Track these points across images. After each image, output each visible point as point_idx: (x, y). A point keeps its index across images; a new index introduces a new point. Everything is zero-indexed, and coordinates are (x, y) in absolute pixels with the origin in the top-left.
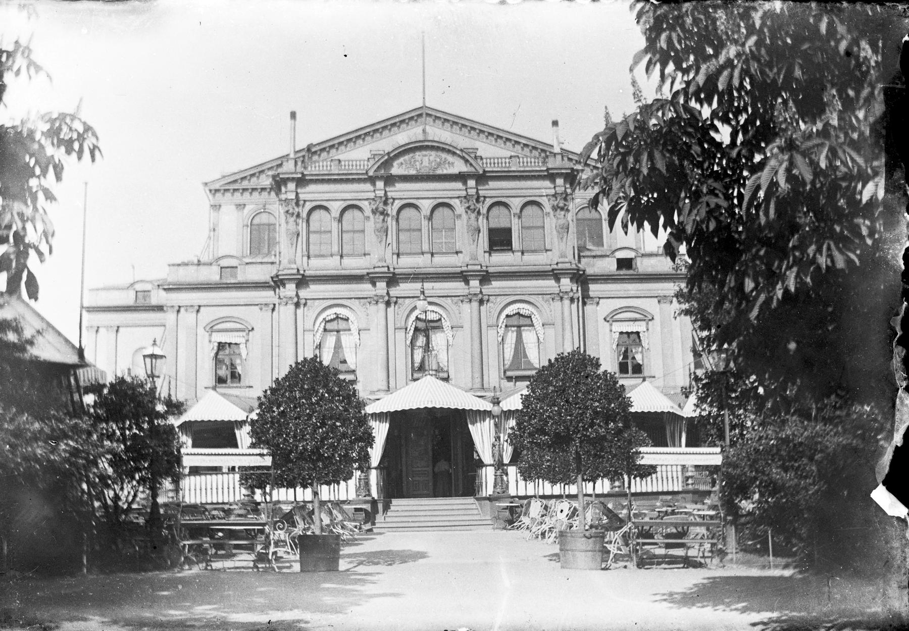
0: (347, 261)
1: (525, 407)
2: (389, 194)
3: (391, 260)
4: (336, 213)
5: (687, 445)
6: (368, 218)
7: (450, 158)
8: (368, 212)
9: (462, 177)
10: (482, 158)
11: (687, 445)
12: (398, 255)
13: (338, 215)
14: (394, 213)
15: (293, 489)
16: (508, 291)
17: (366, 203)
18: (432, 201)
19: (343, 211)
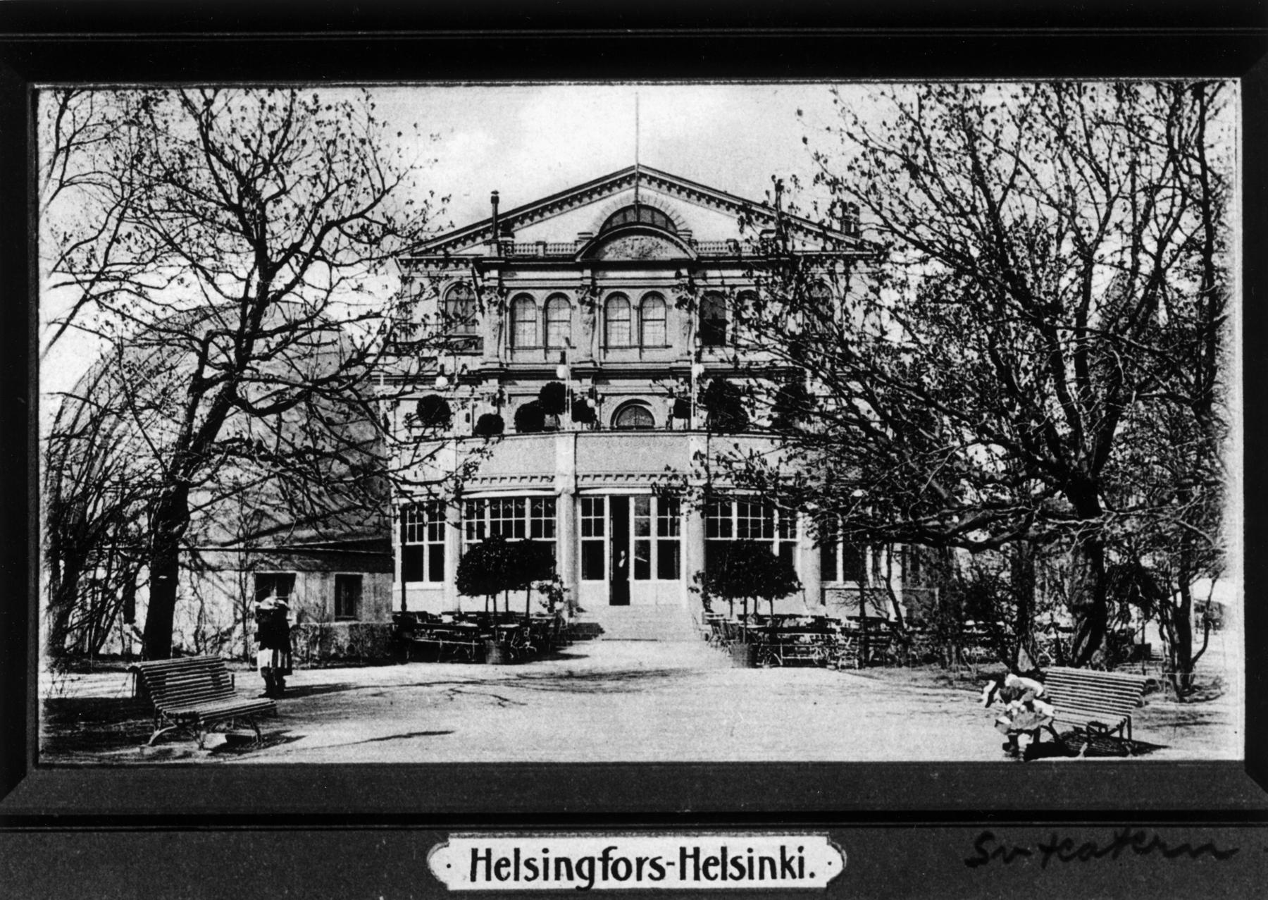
0: (647, 355)
1: (951, 552)
2: (599, 283)
3: (598, 355)
4: (541, 303)
5: (584, 543)
6: (574, 308)
7: (663, 243)
8: (574, 302)
9: (673, 264)
10: (696, 243)
11: (584, 543)
12: (512, 350)
13: (542, 304)
14: (602, 303)
15: (410, 609)
16: (622, 390)
17: (573, 292)
18: (640, 291)
19: (549, 299)
